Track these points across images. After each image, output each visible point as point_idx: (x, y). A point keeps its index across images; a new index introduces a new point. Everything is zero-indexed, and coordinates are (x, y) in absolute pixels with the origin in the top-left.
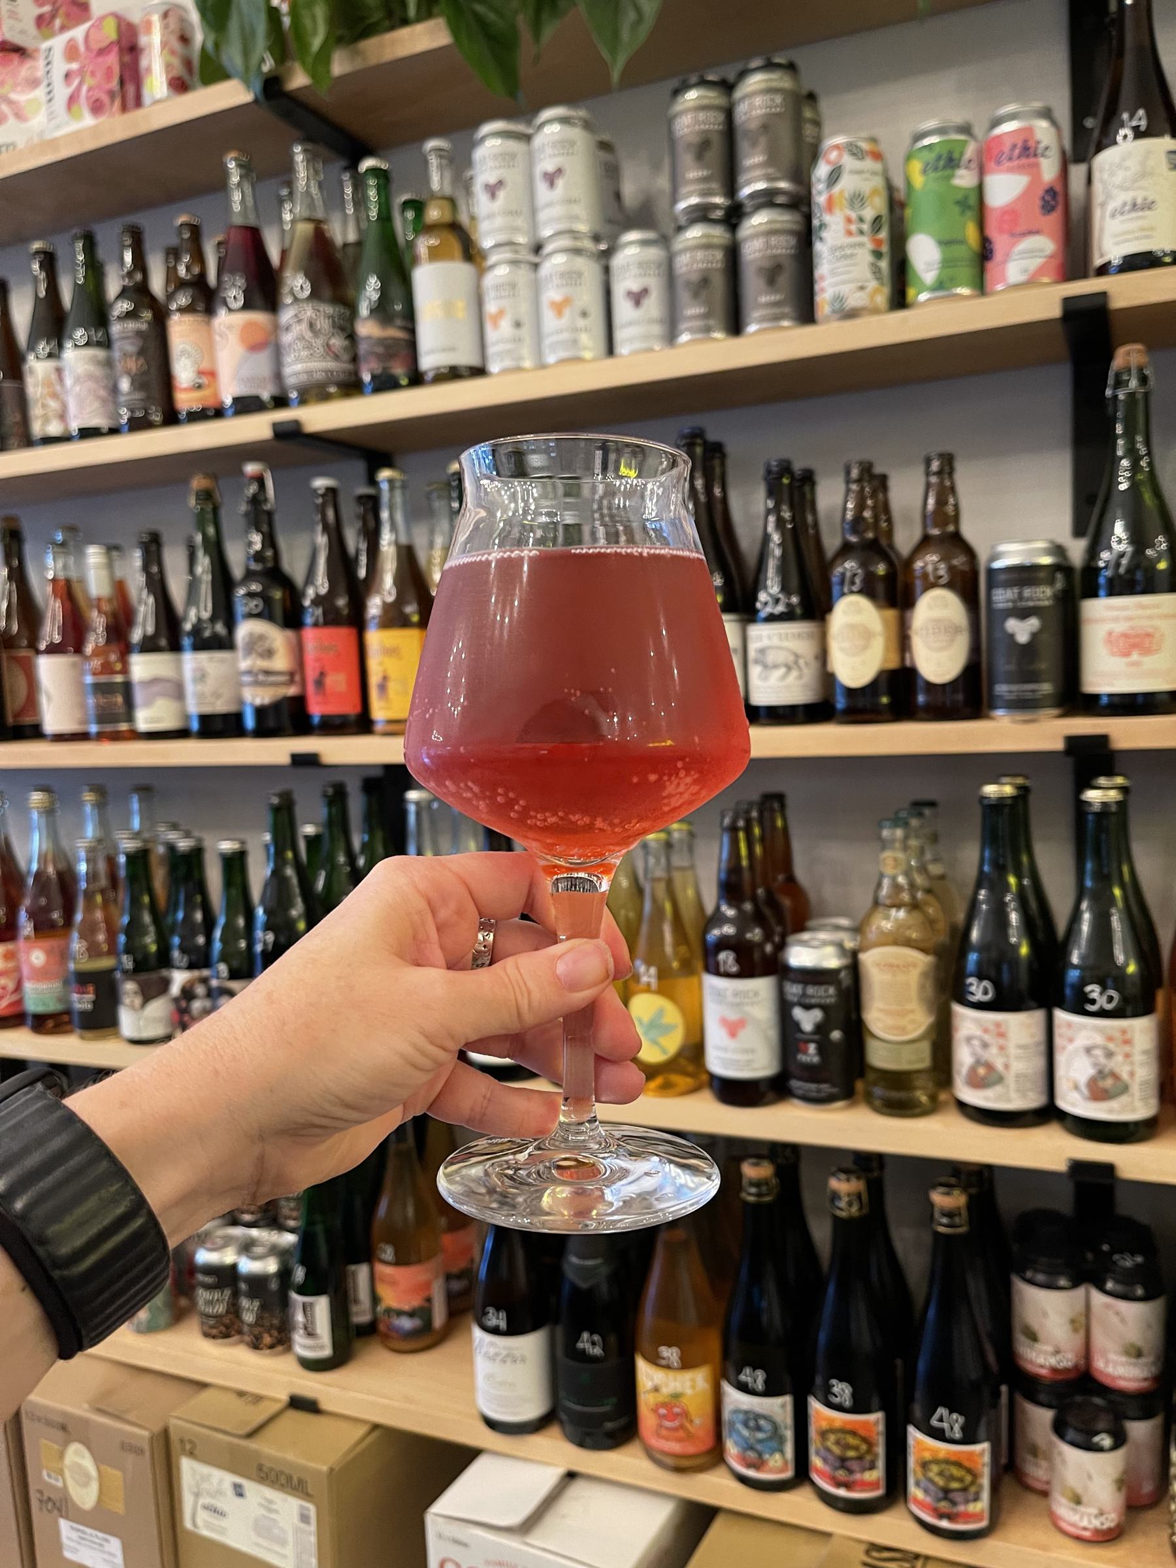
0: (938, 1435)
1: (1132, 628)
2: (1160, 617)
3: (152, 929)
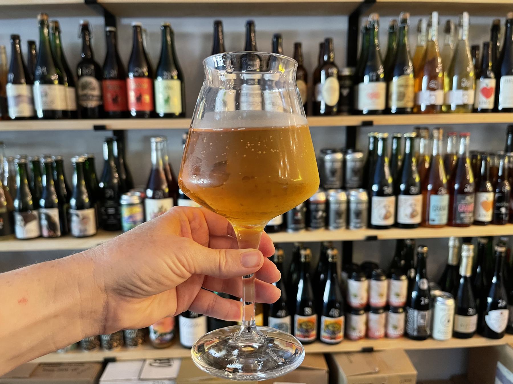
0: (332, 317)
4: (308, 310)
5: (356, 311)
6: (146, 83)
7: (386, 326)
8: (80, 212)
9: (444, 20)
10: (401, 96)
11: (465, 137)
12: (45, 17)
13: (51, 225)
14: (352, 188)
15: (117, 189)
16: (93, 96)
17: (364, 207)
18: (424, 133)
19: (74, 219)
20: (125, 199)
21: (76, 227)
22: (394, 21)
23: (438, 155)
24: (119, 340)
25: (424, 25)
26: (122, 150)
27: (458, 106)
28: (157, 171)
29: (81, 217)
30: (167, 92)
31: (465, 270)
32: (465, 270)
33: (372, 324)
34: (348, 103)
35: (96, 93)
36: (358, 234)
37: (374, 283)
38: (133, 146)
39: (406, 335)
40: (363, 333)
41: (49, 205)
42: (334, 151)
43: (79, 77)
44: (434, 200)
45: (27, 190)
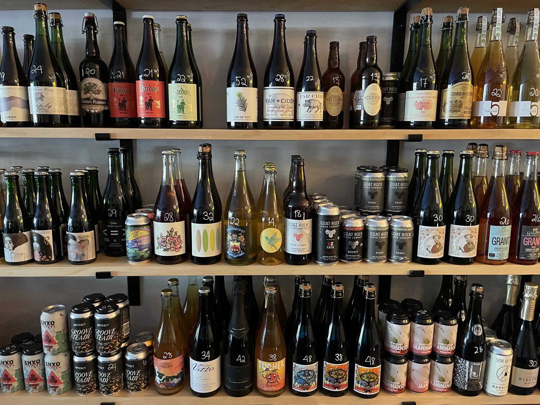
0: (368, 365)
1: (424, 100)
2: (432, 97)
3: (20, 211)
4: (339, 356)
5: (396, 359)
6: (157, 85)
7: (431, 377)
8: (76, 235)
9: (509, 17)
10: (457, 106)
11: (533, 156)
12: (43, 8)
13: (44, 248)
14: (395, 214)
15: (121, 208)
16: (97, 100)
17: (409, 236)
18: (482, 150)
19: (71, 241)
20: (130, 221)
21: (72, 253)
22: (449, 17)
23: (500, 177)
24: (119, 383)
25: (485, 24)
26: (130, 163)
27: (523, 119)
28: (168, 188)
29: (78, 240)
30: (182, 99)
31: (527, 313)
32: (527, 313)
33: (414, 375)
34: (392, 114)
35: (102, 96)
36: (400, 268)
37: (417, 326)
38: (143, 158)
39: (454, 388)
40: (403, 385)
41: (43, 226)
42: (374, 171)
43: (82, 79)
44: (495, 231)
45: (18, 208)
